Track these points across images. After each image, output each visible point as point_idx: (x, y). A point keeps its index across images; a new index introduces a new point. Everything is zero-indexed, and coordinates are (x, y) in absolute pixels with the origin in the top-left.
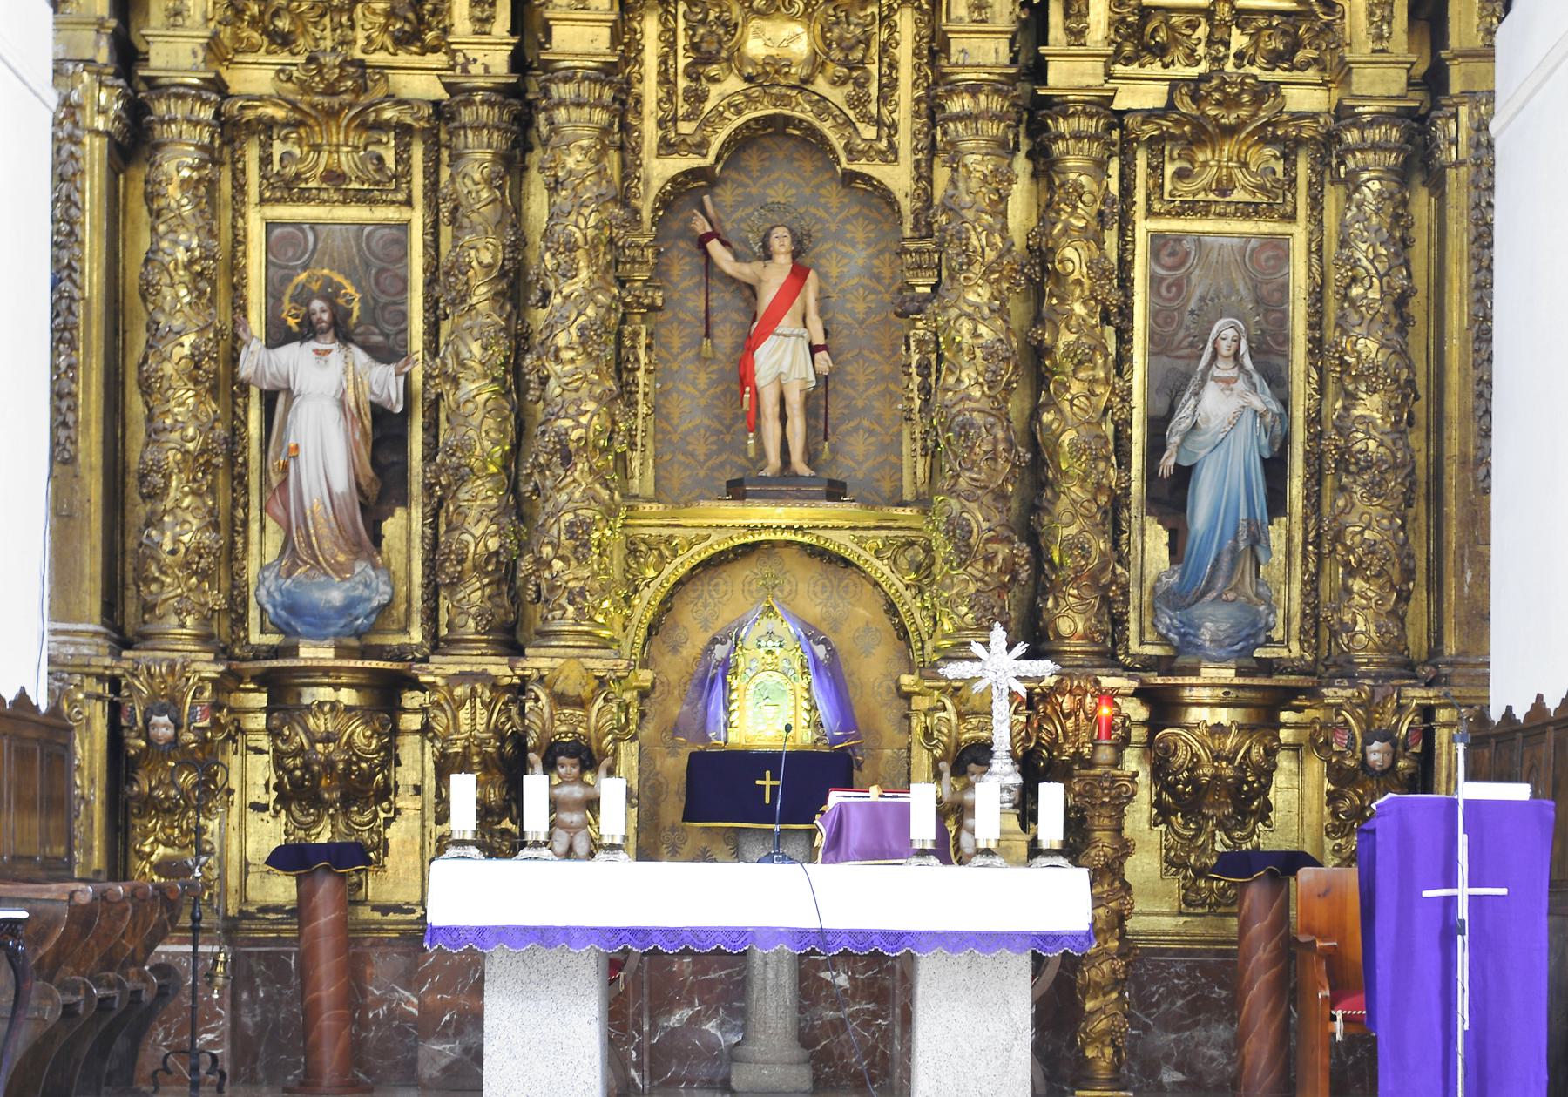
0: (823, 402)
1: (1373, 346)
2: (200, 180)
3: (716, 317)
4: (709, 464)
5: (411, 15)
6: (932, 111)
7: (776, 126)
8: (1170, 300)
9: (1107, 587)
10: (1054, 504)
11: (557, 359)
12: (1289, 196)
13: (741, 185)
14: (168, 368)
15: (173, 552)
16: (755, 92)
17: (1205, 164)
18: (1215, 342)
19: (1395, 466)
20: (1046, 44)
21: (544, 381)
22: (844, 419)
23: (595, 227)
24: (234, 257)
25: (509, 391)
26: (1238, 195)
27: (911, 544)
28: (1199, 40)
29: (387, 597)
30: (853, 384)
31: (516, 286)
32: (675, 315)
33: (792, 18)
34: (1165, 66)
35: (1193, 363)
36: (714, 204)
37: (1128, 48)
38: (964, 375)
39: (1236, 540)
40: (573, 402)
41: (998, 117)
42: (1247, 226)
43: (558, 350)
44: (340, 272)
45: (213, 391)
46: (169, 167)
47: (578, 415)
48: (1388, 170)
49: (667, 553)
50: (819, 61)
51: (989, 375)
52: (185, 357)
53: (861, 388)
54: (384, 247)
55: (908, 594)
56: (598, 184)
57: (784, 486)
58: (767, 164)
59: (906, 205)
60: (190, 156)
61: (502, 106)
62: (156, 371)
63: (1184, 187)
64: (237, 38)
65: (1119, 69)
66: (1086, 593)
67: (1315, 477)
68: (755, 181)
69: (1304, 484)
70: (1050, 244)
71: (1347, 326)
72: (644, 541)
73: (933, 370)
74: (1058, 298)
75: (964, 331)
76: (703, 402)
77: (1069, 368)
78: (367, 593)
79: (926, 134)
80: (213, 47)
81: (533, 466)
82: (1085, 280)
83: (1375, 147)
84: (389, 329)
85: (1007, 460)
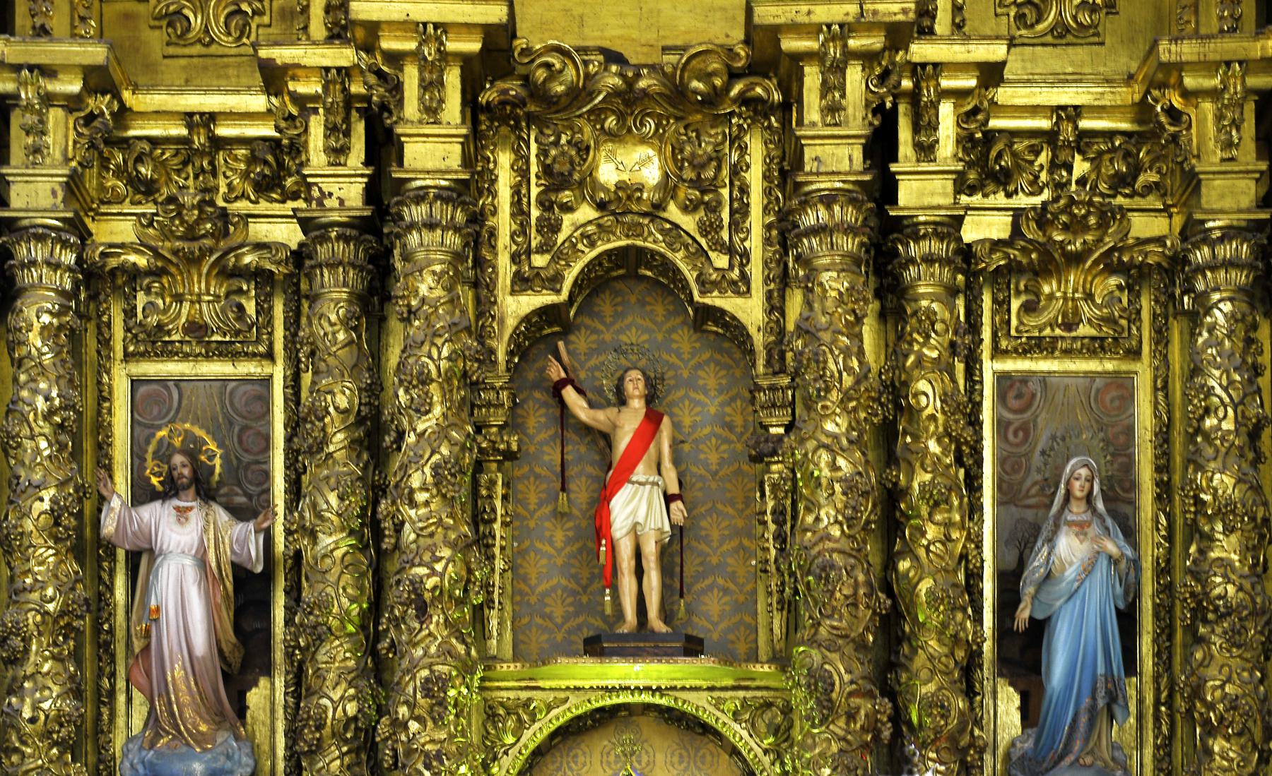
0: (678, 560)
1: (1229, 481)
2: (61, 327)
3: (571, 472)
4: (566, 627)
5: (270, 158)
6: (785, 232)
7: (628, 262)
8: (1017, 445)
9: (965, 751)
10: (911, 660)
11: (413, 504)
12: (1134, 331)
13: (595, 331)
14: (29, 525)
15: (33, 720)
16: (608, 220)
17: (1051, 297)
18: (1068, 483)
19: (1254, 614)
20: (896, 160)
21: (399, 528)
22: (700, 576)
23: (449, 359)
24: (99, 413)
25: (367, 546)
26: (1084, 330)
27: (768, 705)
28: (1042, 166)
29: (249, 770)
30: (707, 539)
31: (375, 435)
32: (531, 470)
33: (643, 140)
34: (1009, 195)
35: (1041, 512)
36: (568, 352)
37: (972, 176)
38: (823, 513)
39: (1094, 698)
40: (427, 548)
41: (850, 230)
42: (1092, 365)
43: (412, 491)
44: (201, 427)
45: (78, 552)
46: (30, 312)
47: (437, 570)
48: (1240, 289)
49: (525, 717)
50: (671, 184)
51: (849, 512)
52: (45, 512)
53: (715, 544)
54: (246, 404)
55: (766, 760)
56: (452, 314)
57: (641, 643)
58: (620, 309)
59: (759, 339)
60: (49, 301)
61: (358, 242)
62: (15, 527)
63: (1031, 321)
64: (102, 188)
65: (964, 199)
66: (945, 756)
67: (1165, 633)
68: (608, 327)
69: (1154, 641)
70: (903, 377)
71: (1201, 461)
72: (502, 704)
73: (788, 518)
74: (912, 436)
75: (823, 465)
76: (559, 561)
77: (924, 511)
78: (229, 765)
79: (778, 262)
80: (73, 186)
81: (389, 619)
82: (939, 415)
83: (1229, 264)
84: (252, 489)
85: (868, 607)
